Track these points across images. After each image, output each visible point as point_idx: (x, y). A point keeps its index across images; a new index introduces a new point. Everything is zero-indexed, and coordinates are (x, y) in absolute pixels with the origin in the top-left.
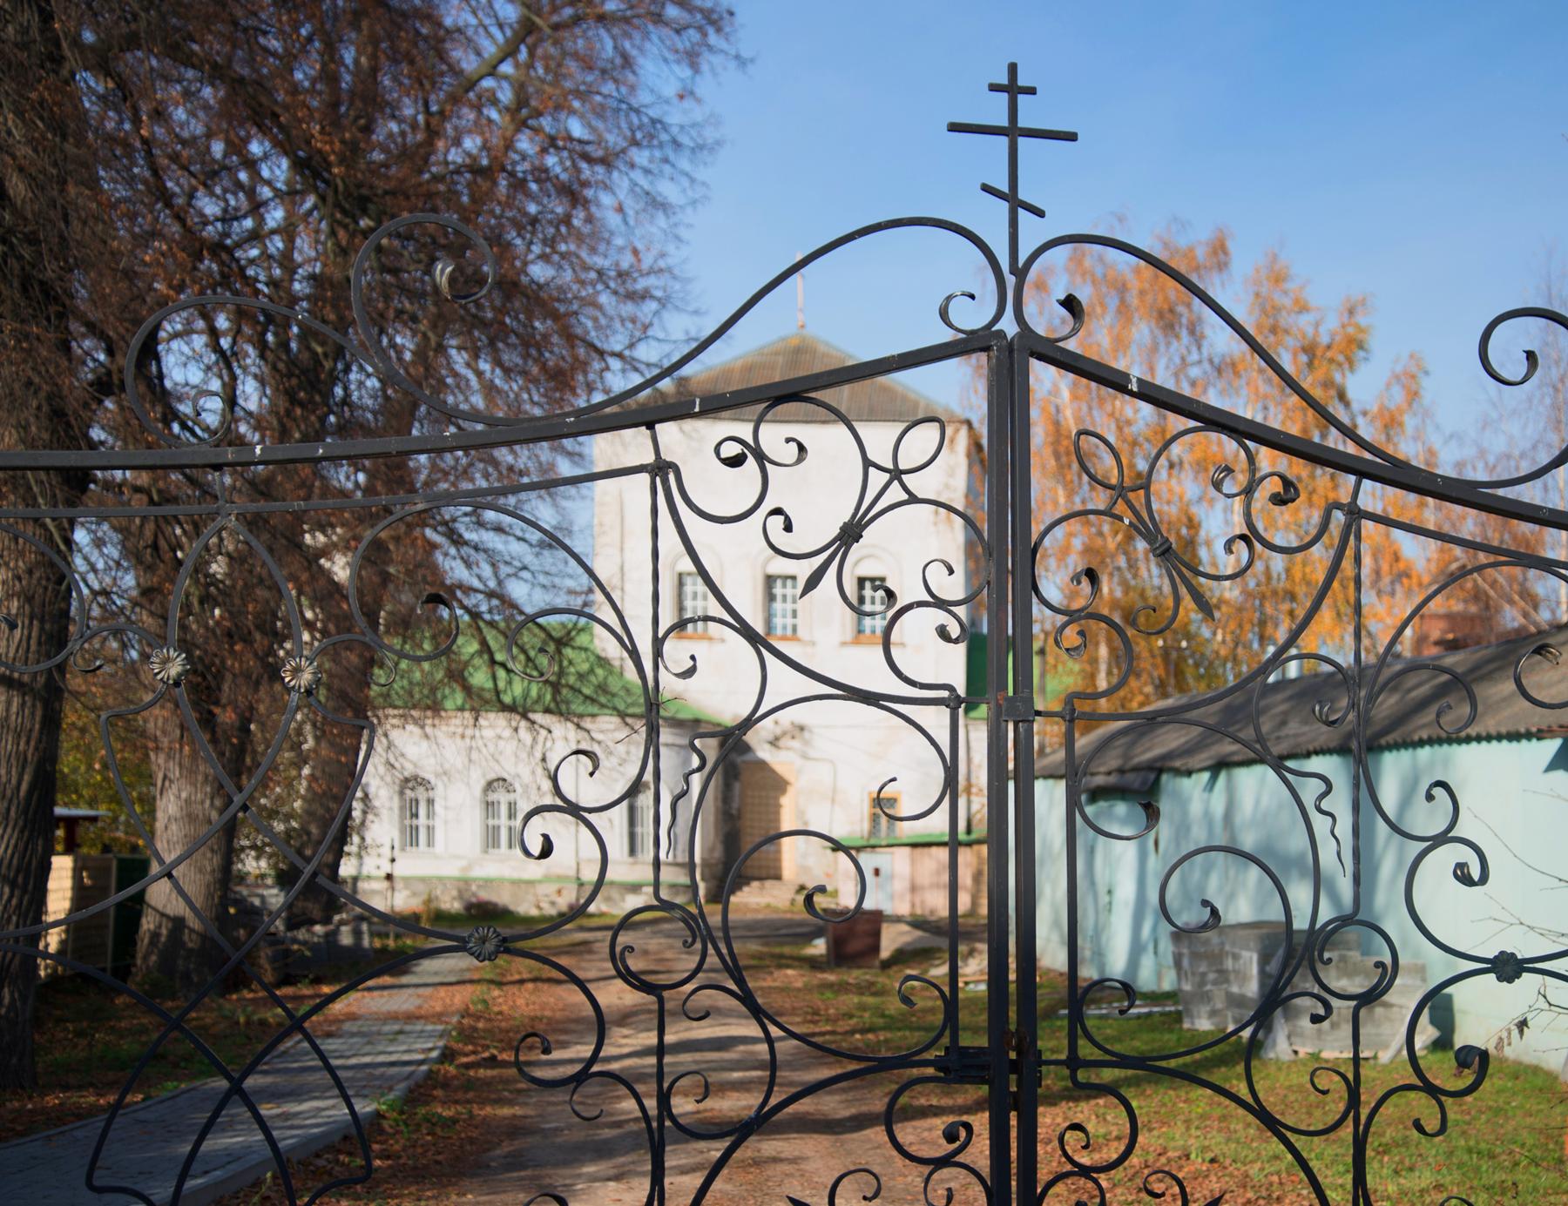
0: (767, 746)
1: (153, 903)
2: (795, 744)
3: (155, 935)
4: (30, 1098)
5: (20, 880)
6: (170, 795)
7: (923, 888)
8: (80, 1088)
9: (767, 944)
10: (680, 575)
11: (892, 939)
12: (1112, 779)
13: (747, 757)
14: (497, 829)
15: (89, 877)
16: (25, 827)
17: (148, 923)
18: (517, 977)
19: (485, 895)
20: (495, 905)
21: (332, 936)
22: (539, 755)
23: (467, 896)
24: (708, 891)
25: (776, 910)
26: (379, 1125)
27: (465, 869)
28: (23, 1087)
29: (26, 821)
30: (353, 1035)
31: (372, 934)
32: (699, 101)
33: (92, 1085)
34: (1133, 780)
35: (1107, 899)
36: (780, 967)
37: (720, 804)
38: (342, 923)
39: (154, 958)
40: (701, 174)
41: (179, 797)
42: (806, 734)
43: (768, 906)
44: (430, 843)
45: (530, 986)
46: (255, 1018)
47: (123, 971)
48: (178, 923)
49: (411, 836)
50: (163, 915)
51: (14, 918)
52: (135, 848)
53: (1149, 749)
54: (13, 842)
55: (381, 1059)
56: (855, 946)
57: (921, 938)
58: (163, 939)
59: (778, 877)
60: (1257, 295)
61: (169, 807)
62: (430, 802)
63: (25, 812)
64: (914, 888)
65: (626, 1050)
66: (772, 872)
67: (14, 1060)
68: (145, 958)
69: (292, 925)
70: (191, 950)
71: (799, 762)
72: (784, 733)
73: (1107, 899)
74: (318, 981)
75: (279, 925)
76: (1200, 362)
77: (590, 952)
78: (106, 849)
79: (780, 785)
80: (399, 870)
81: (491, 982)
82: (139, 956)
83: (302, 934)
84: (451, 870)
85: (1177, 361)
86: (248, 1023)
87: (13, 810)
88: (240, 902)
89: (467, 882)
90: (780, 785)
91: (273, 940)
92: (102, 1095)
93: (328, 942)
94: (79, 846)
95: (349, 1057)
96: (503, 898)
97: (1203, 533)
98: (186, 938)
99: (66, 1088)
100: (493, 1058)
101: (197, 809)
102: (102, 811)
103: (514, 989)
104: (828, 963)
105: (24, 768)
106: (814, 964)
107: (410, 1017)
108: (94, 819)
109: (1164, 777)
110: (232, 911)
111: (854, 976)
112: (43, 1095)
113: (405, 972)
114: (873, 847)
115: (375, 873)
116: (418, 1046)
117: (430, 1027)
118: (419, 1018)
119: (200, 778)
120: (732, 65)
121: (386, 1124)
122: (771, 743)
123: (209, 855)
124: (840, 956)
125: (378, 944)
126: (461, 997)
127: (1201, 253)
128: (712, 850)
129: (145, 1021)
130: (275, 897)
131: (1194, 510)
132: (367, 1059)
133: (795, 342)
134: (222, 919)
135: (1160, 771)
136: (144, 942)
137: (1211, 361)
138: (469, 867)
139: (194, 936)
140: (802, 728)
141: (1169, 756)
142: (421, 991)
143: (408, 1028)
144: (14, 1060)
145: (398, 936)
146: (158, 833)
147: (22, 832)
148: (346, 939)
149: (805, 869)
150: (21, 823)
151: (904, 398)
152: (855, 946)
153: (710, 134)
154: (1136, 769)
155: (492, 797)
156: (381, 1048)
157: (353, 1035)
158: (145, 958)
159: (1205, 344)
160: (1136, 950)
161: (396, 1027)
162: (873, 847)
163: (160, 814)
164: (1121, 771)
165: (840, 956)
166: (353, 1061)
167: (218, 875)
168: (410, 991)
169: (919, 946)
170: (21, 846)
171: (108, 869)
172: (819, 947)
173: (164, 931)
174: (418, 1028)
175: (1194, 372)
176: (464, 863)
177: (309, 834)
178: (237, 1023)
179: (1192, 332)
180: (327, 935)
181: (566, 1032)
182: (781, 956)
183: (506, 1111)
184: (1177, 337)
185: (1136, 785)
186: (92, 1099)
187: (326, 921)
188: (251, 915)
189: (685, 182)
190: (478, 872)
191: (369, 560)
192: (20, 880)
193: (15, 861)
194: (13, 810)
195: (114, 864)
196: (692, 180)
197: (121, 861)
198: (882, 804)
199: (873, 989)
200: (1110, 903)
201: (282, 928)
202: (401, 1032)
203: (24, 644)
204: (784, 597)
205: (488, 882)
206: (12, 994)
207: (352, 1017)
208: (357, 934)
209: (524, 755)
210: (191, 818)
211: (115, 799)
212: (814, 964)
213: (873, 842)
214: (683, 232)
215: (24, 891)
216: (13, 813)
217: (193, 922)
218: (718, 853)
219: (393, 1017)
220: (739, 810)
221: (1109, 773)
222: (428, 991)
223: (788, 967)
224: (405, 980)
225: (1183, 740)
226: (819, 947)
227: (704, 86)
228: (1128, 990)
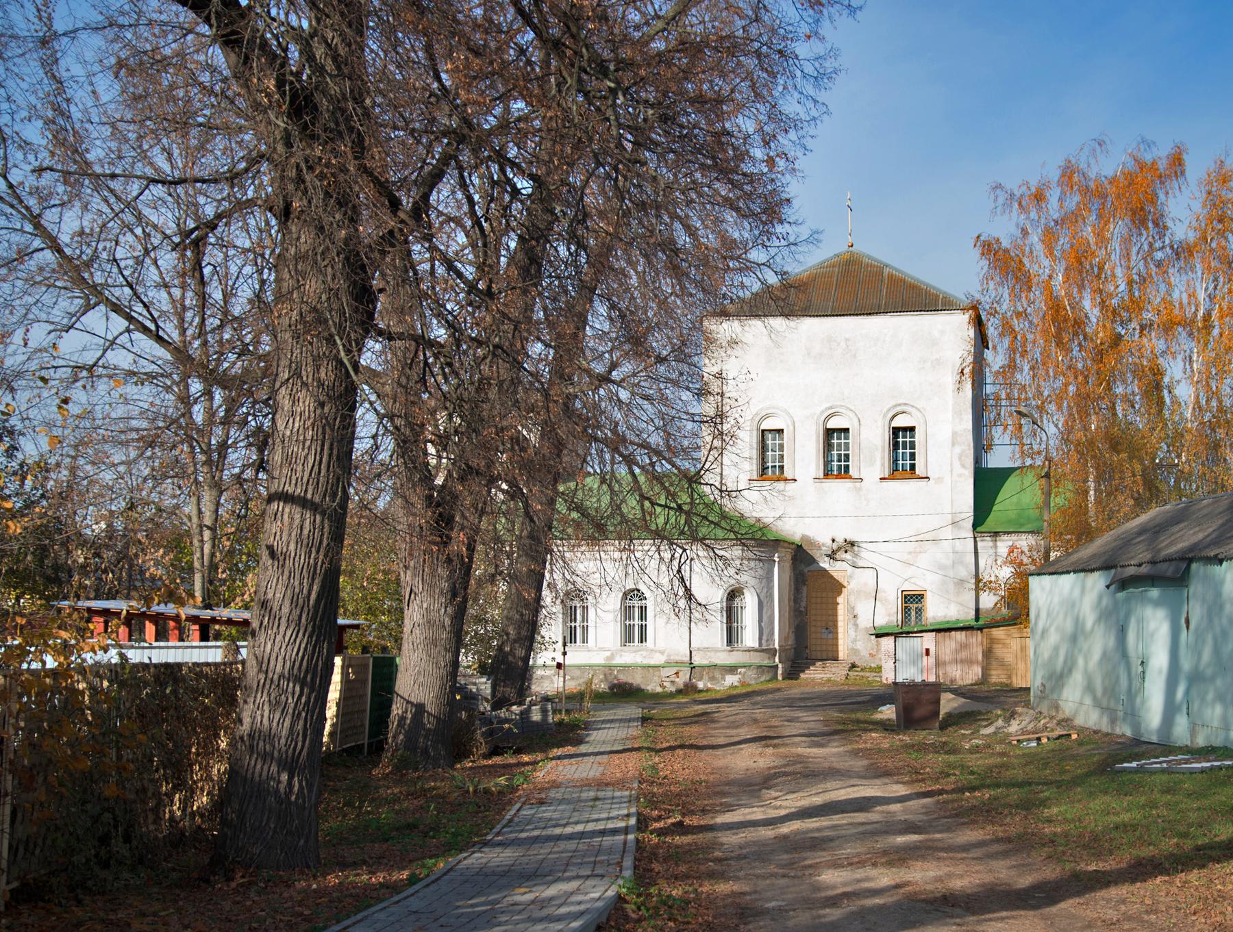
0: (827, 559)
1: (401, 693)
2: (848, 556)
3: (402, 719)
4: (315, 877)
5: (309, 678)
6: (415, 605)
7: (945, 663)
8: (355, 865)
9: (841, 712)
10: (763, 431)
11: (948, 704)
12: (1144, 570)
13: (812, 568)
14: (631, 627)
15: (354, 673)
16: (313, 631)
17: (397, 709)
18: (666, 745)
19: (623, 678)
20: (631, 685)
21: (525, 714)
22: (675, 569)
23: (610, 678)
24: (784, 669)
25: (835, 683)
26: (623, 909)
27: (608, 658)
28: (308, 867)
29: (314, 627)
30: (561, 801)
31: (555, 712)
32: (822, 39)
33: (364, 862)
34: (1168, 569)
35: (1140, 669)
36: (866, 730)
37: (792, 604)
38: (532, 704)
39: (401, 737)
40: (822, 96)
41: (421, 607)
42: (856, 548)
43: (829, 680)
44: (585, 640)
45: (680, 752)
46: (481, 787)
47: (377, 747)
48: (420, 708)
49: (570, 637)
50: (408, 702)
51: (304, 714)
52: (384, 649)
53: (1171, 544)
54: (303, 646)
55: (591, 827)
56: (920, 712)
57: (964, 704)
58: (408, 722)
59: (836, 659)
60: (1209, 193)
61: (413, 615)
62: (585, 609)
63: (314, 618)
64: (938, 664)
65: (783, 812)
66: (830, 655)
67: (302, 842)
68: (394, 737)
69: (495, 707)
70: (429, 730)
71: (850, 569)
72: (839, 549)
73: (1140, 669)
74: (519, 751)
75: (485, 707)
76: (1163, 247)
77: (713, 721)
78: (365, 650)
79: (837, 587)
80: (569, 660)
81: (650, 749)
82: (390, 735)
83: (503, 713)
84: (599, 659)
85: (1146, 247)
86: (475, 791)
87: (304, 616)
88: (462, 689)
89: (610, 667)
90: (837, 587)
91: (487, 721)
92: (373, 873)
93: (522, 718)
94: (346, 648)
95: (565, 826)
96: (637, 679)
97: (1166, 380)
98: (426, 720)
99: (343, 866)
100: (680, 824)
101: (434, 616)
102: (361, 621)
103: (667, 755)
104: (898, 726)
105: (313, 579)
106: (885, 726)
107: (601, 784)
108: (357, 627)
109: (1194, 566)
110: (458, 697)
111: (920, 736)
112: (324, 875)
113: (579, 741)
114: (908, 633)
115: (549, 663)
116: (614, 813)
117: (618, 794)
118: (607, 785)
119: (437, 591)
120: (846, 12)
121: (630, 907)
122: (829, 556)
123: (443, 653)
124: (908, 720)
125: (557, 718)
126: (632, 764)
127: (1162, 165)
128: (786, 639)
129: (396, 791)
130: (484, 686)
131: (1161, 361)
132: (580, 828)
133: (847, 256)
134: (451, 703)
135: (1191, 561)
136: (393, 725)
137: (1172, 247)
138: (612, 657)
139: (431, 719)
140: (852, 544)
141: (1192, 548)
142: (599, 758)
143: (601, 794)
144: (302, 842)
145: (568, 712)
146: (405, 636)
147: (311, 636)
148: (536, 716)
149: (855, 651)
150: (310, 629)
151: (927, 293)
152: (920, 712)
153: (829, 65)
154: (1168, 560)
155: (628, 603)
156: (586, 816)
157: (561, 801)
158: (394, 736)
159: (1168, 233)
160: (1170, 709)
161: (592, 794)
162: (908, 633)
163: (407, 621)
164: (1153, 562)
165: (908, 720)
166: (569, 830)
167: (449, 669)
168: (591, 759)
169: (964, 710)
170: (310, 649)
171: (366, 666)
172: (888, 712)
173: (409, 716)
174: (609, 794)
175: (1159, 255)
176: (608, 654)
177: (507, 634)
178: (468, 792)
179: (1156, 225)
180: (522, 713)
181: (724, 794)
182: (858, 721)
183: (723, 888)
184: (1147, 228)
185: (1169, 574)
186: (365, 877)
187: (520, 703)
188: (471, 698)
189: (810, 104)
190: (618, 660)
191: (142, 716)
192: (309, 678)
193: (305, 663)
194: (304, 616)
195: (371, 660)
196: (815, 102)
197: (375, 659)
198: (912, 600)
199: (946, 749)
200: (1144, 672)
201: (489, 708)
202: (596, 799)
203: (316, 467)
204: (839, 445)
205: (625, 667)
206: (300, 784)
207: (555, 785)
208: (544, 711)
209: (664, 568)
210: (430, 623)
211: (371, 611)
212: (885, 726)
213: (905, 629)
214: (809, 142)
215: (312, 690)
216: (303, 620)
217: (432, 708)
218: (791, 642)
219: (587, 784)
220: (806, 608)
221: (1140, 565)
222: (605, 757)
223: (871, 731)
224: (583, 749)
225: (1201, 536)
226: (888, 712)
227: (826, 29)
228: (1165, 748)
